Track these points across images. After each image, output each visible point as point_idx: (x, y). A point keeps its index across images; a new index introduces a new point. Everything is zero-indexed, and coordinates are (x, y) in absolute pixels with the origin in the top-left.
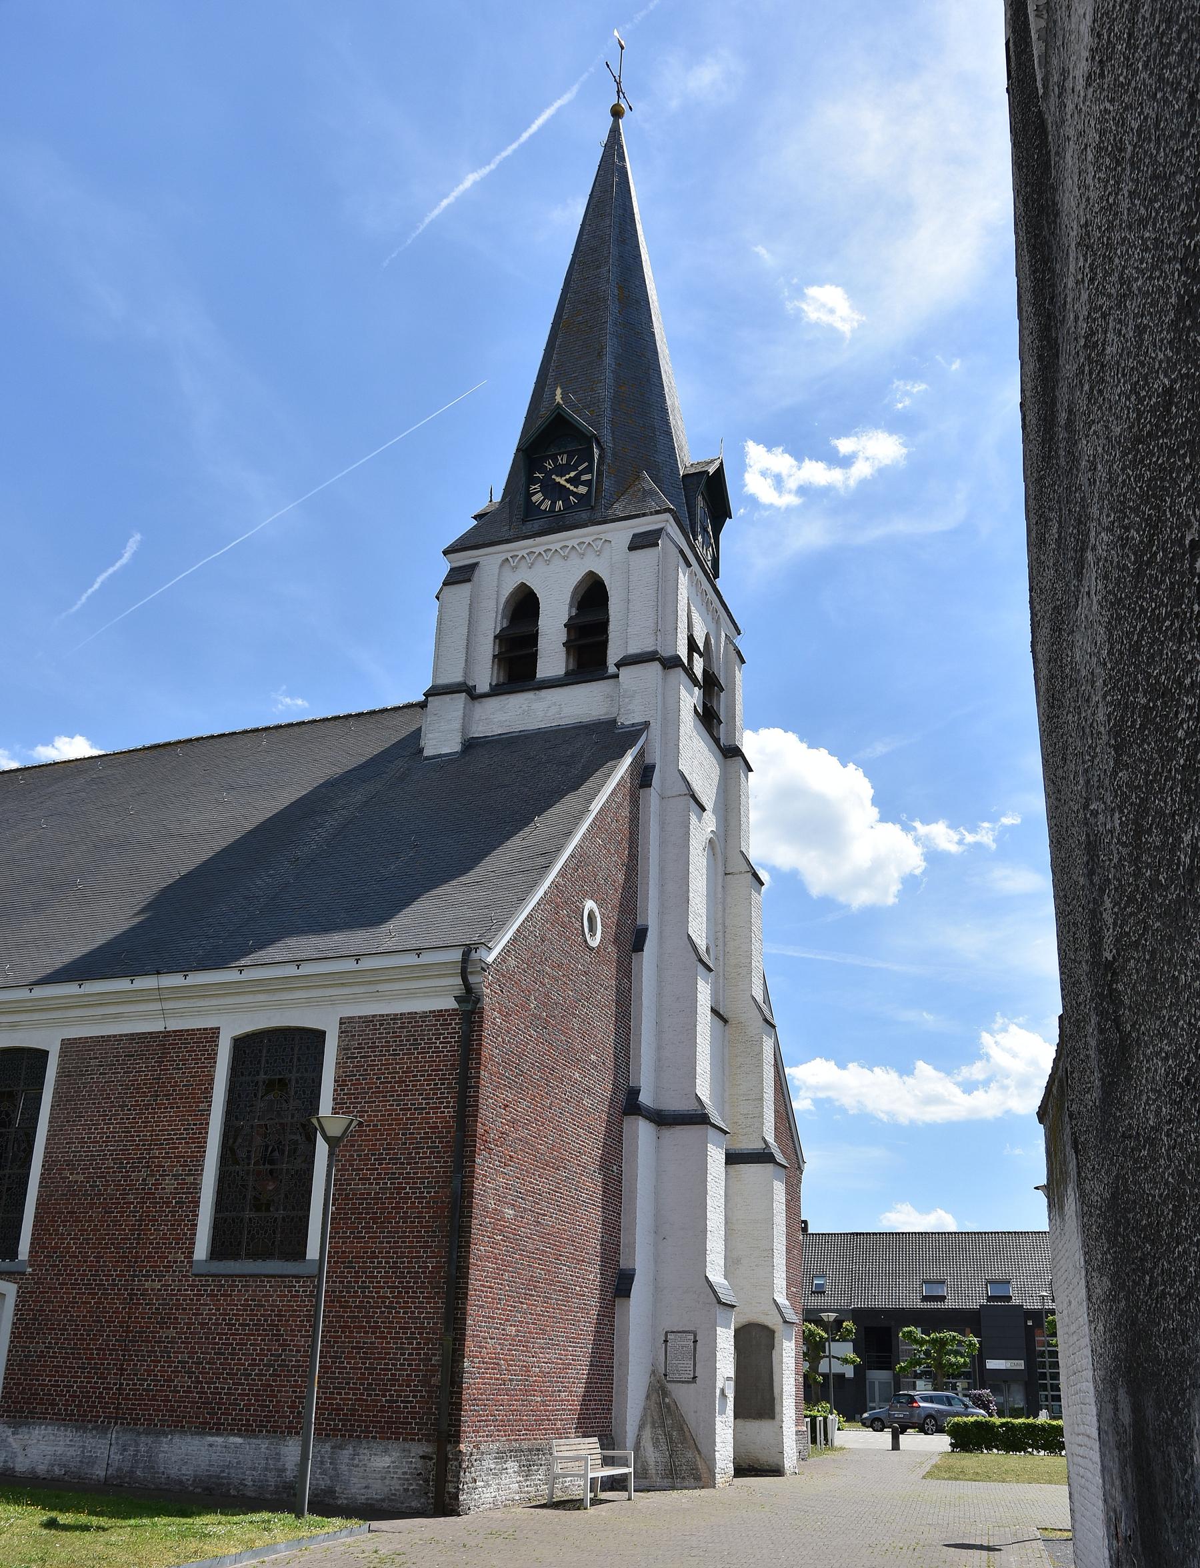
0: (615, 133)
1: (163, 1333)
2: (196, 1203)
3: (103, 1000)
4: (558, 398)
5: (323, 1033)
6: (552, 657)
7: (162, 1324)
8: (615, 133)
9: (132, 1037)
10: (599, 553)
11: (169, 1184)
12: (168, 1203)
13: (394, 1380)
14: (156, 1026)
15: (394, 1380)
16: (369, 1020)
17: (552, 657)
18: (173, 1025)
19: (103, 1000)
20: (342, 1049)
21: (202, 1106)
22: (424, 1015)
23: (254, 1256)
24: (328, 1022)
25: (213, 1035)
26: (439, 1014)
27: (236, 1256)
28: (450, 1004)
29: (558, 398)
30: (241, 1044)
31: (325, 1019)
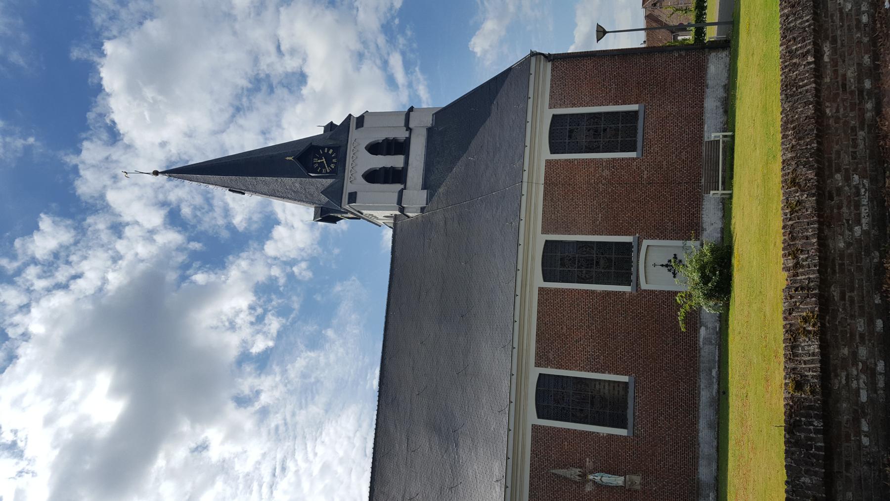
0: (163, 173)
1: (665, 166)
2: (614, 159)
3: (528, 210)
4: (290, 158)
5: (547, 241)
6: (397, 161)
7: (661, 168)
8: (163, 173)
9: (545, 199)
10: (359, 144)
11: (606, 173)
12: (613, 172)
13: (684, 70)
14: (542, 188)
15: (684, 70)
16: (551, 97)
17: (397, 161)
18: (542, 181)
19: (528, 210)
20: (561, 106)
21: (576, 162)
22: (552, 76)
23: (635, 135)
24: (534, 373)
25: (534, 427)
26: (553, 70)
27: (635, 142)
28: (549, 65)
29: (290, 158)
30: (540, 416)
31: (540, 240)
